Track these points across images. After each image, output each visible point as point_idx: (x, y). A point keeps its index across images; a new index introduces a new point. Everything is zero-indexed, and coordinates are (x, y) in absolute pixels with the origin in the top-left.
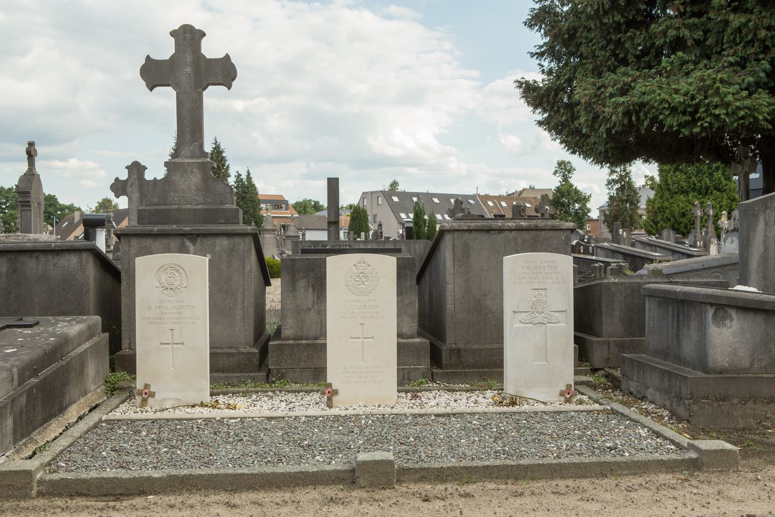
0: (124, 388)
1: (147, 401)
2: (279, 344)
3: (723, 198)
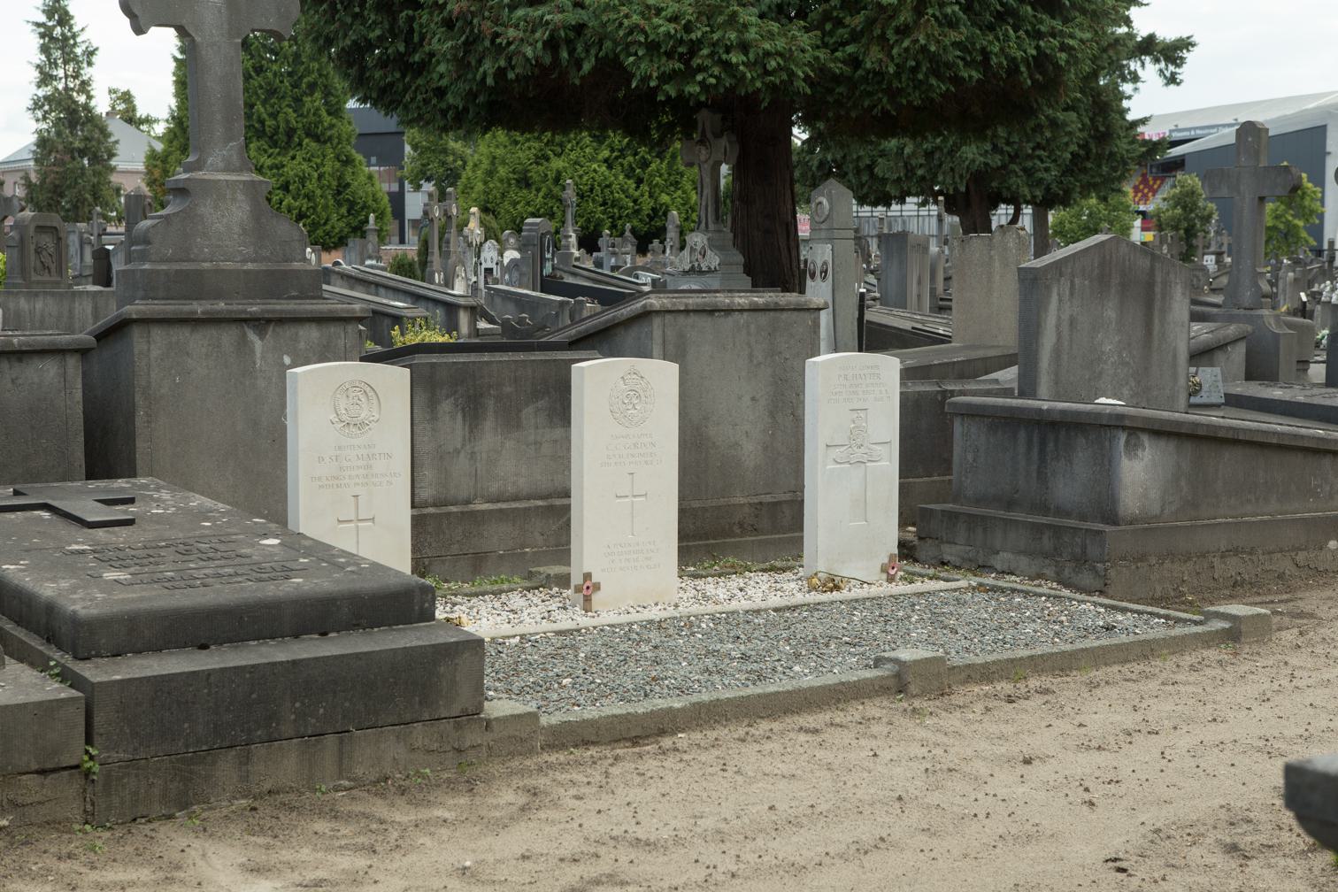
3: (324, 156)
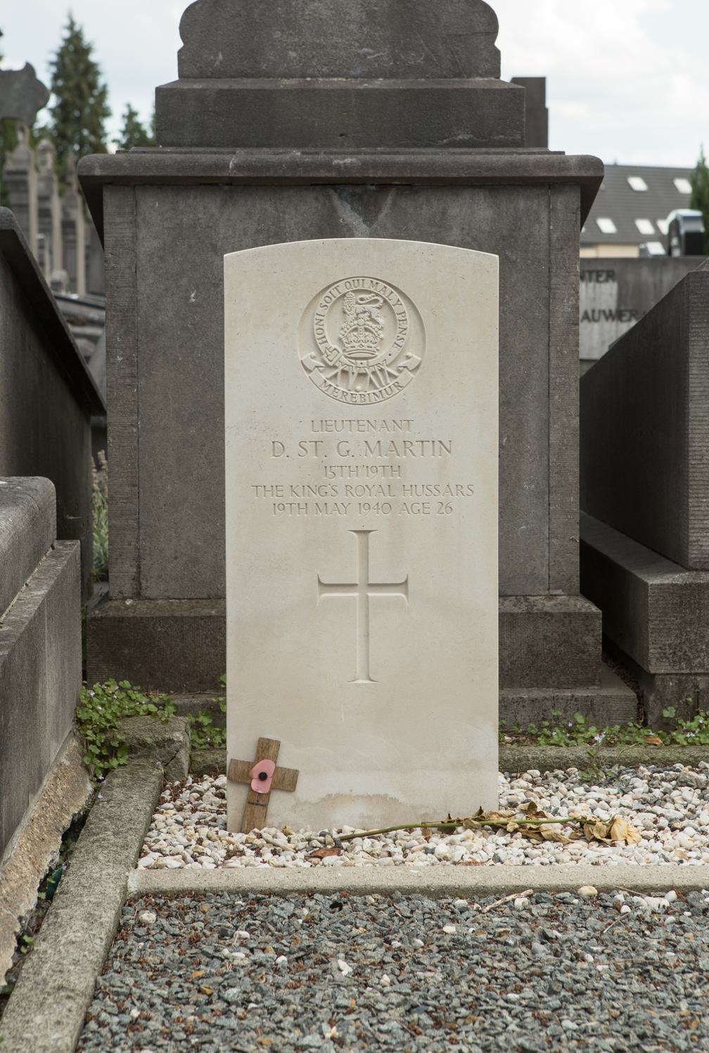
0: (144, 744)
1: (265, 806)
2: (686, 586)
